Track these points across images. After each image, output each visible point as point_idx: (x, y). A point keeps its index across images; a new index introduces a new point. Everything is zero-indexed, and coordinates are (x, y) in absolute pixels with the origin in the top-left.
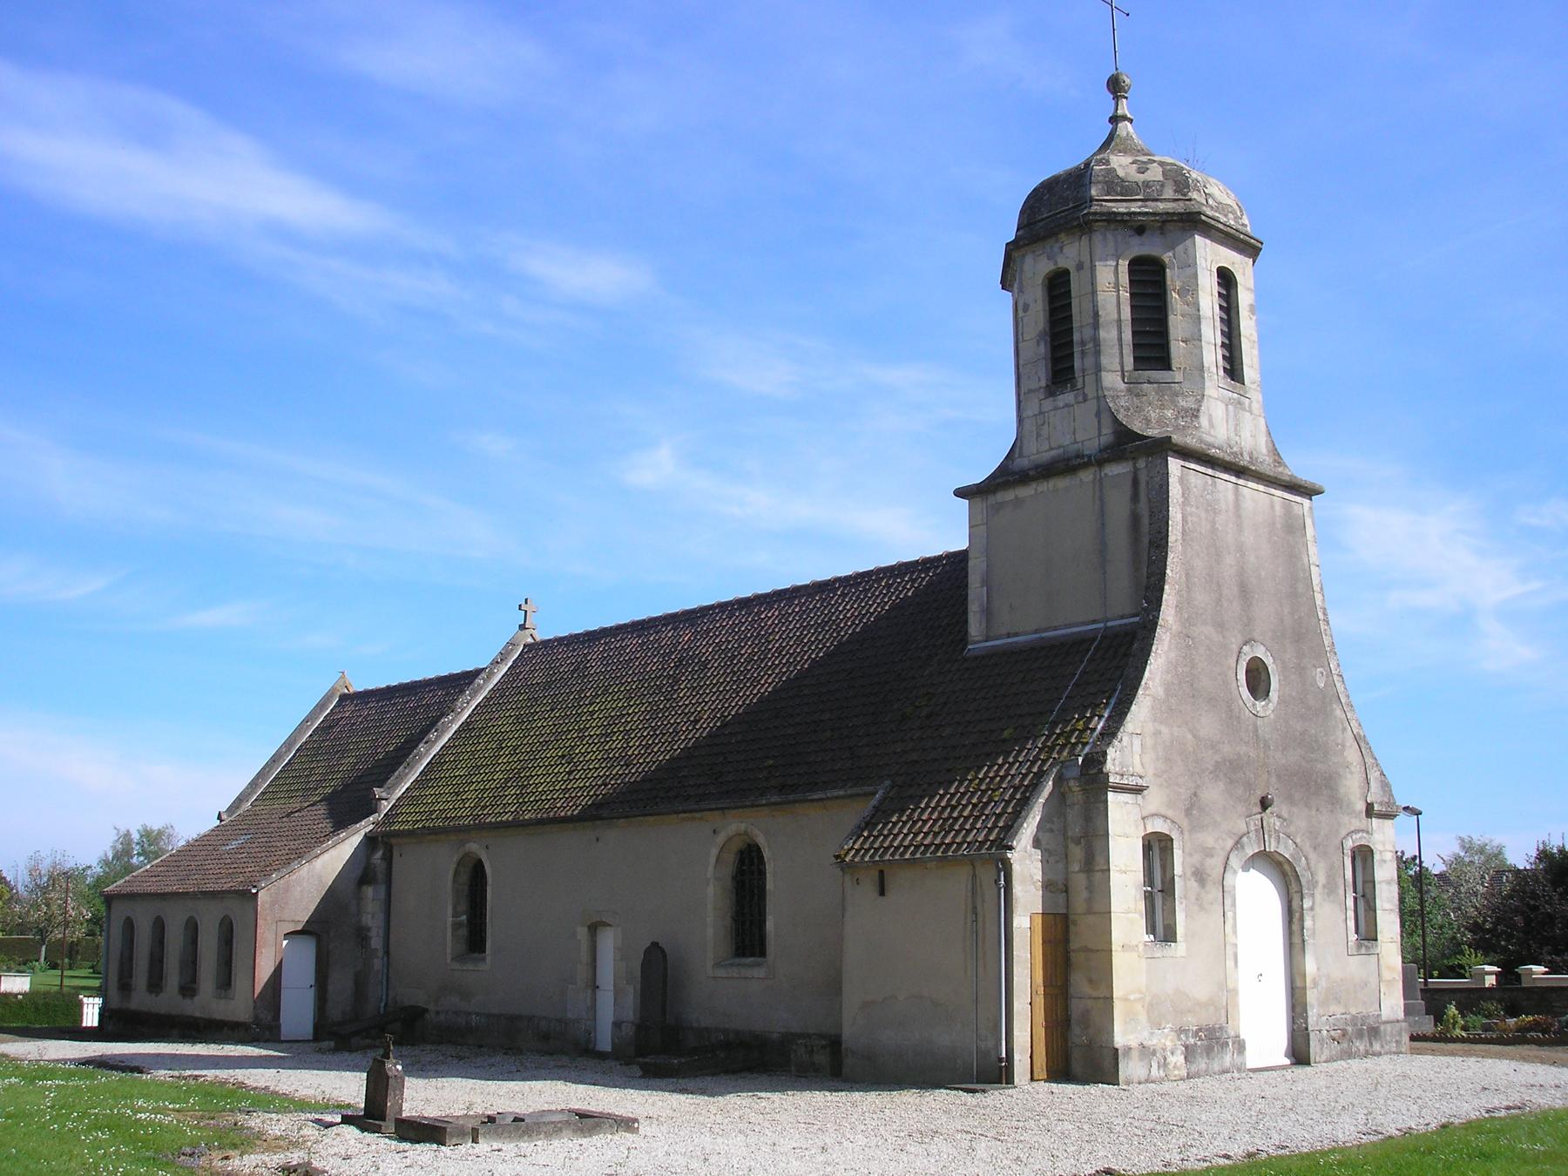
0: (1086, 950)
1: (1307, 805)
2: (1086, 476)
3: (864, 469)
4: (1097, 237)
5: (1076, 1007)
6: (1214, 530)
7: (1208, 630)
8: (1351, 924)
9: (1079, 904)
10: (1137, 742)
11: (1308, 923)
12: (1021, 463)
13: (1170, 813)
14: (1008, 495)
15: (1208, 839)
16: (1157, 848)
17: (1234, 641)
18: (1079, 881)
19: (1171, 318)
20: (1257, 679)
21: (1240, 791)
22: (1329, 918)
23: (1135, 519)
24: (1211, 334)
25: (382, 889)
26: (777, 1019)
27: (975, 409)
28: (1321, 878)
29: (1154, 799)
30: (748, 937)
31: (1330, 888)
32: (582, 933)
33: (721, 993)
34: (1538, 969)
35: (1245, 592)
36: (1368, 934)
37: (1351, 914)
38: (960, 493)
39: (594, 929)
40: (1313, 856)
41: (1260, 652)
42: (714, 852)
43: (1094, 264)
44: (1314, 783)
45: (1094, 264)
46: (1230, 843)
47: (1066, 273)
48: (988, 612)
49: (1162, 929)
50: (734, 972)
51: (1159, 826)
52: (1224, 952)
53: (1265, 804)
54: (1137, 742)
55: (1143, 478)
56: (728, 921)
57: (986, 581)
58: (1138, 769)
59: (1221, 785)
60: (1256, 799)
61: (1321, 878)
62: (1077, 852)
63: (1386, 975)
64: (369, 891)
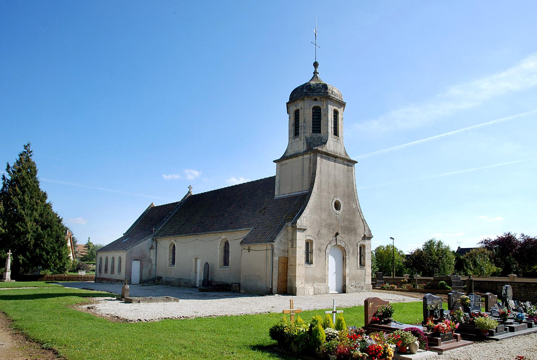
0: (291, 265)
1: (349, 235)
2: (300, 157)
3: (255, 154)
4: (306, 101)
5: (289, 278)
6: (328, 171)
7: (325, 194)
8: (359, 262)
9: (290, 255)
10: (305, 219)
11: (347, 261)
12: (287, 155)
13: (313, 235)
14: (284, 162)
15: (322, 241)
16: (308, 244)
17: (332, 197)
18: (290, 250)
19: (322, 121)
20: (337, 206)
21: (331, 231)
22: (353, 261)
23: (310, 168)
24: (331, 125)
25: (155, 250)
26: (230, 280)
27: (279, 141)
28: (351, 251)
29: (308, 232)
30: (226, 262)
31: (353, 254)
32: (194, 260)
33: (221, 274)
34: (418, 276)
35: (335, 186)
36: (362, 264)
37: (359, 260)
38: (275, 161)
39: (196, 259)
40: (349, 246)
41: (339, 199)
42: (219, 242)
43: (312, 108)
44: (351, 230)
45: (312, 108)
46: (328, 242)
47: (299, 110)
48: (279, 189)
49: (308, 261)
50: (223, 269)
51: (310, 238)
52: (325, 267)
53: (337, 234)
54: (305, 219)
55: (312, 158)
56: (222, 258)
57: (279, 182)
58: (305, 225)
59: (326, 229)
60: (335, 233)
61: (351, 251)
62: (290, 243)
63: (367, 274)
64: (152, 250)
